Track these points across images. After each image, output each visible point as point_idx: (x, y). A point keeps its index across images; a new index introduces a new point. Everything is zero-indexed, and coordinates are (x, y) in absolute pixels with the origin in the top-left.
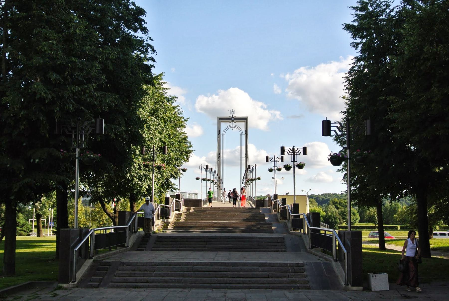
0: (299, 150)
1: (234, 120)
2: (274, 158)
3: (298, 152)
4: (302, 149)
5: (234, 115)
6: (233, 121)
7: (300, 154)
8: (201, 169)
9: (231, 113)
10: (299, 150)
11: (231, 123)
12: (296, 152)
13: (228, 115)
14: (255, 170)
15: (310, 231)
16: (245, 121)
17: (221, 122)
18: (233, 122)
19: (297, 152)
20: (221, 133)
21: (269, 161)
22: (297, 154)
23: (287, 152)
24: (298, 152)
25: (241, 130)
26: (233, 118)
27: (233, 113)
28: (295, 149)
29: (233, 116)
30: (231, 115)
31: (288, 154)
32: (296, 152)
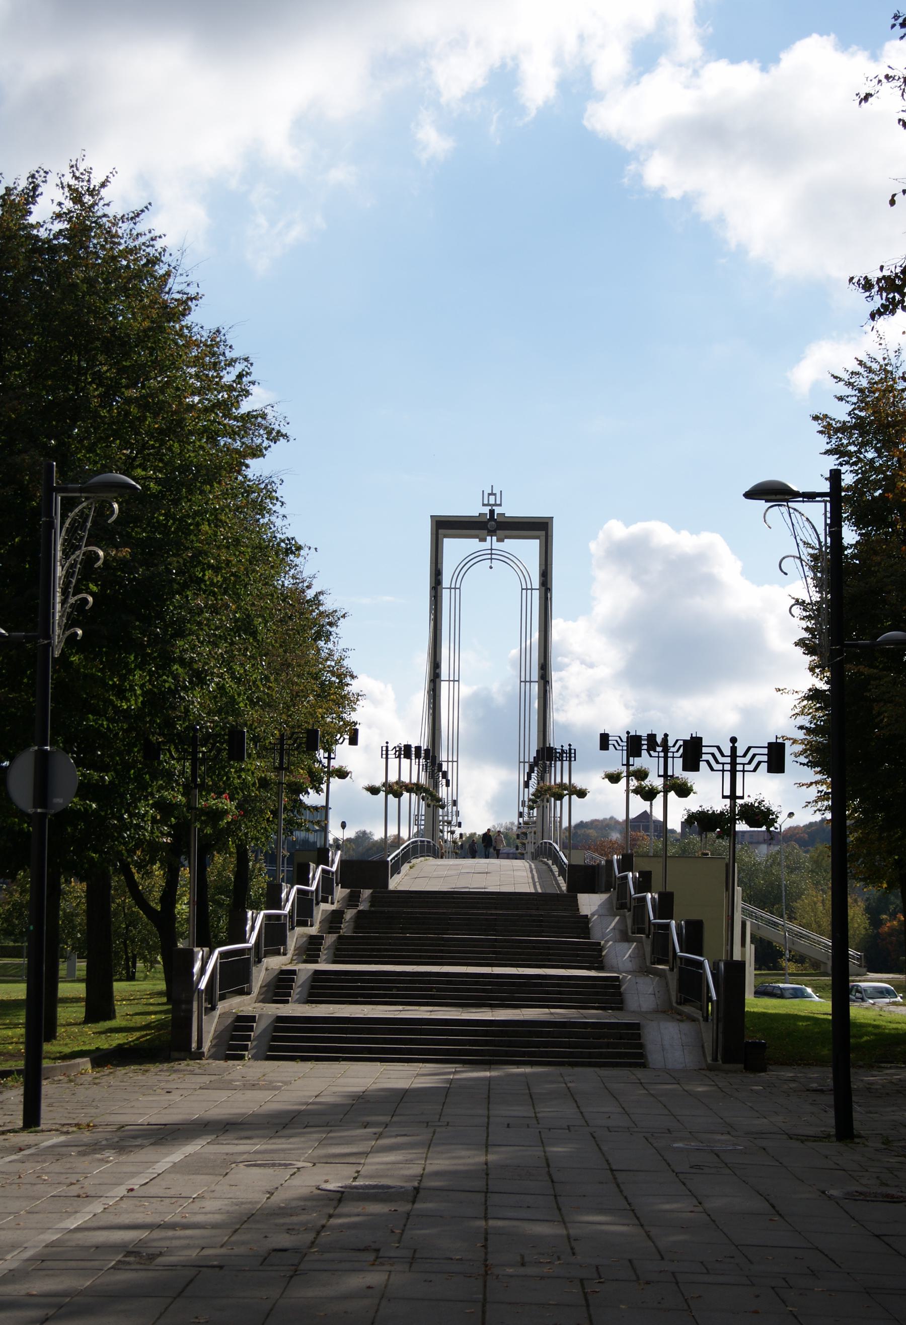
0: (754, 756)
2: (727, 752)
3: (750, 763)
4: (765, 751)
5: (498, 510)
6: (492, 533)
9: (486, 502)
10: (754, 756)
11: (484, 540)
12: (672, 749)
13: (473, 509)
15: (652, 927)
16: (543, 533)
18: (494, 538)
19: (675, 749)
21: (611, 747)
23: (614, 745)
24: (750, 763)
25: (525, 575)
27: (492, 501)
28: (670, 743)
29: (492, 512)
30: (486, 510)
31: (616, 749)
32: (672, 749)
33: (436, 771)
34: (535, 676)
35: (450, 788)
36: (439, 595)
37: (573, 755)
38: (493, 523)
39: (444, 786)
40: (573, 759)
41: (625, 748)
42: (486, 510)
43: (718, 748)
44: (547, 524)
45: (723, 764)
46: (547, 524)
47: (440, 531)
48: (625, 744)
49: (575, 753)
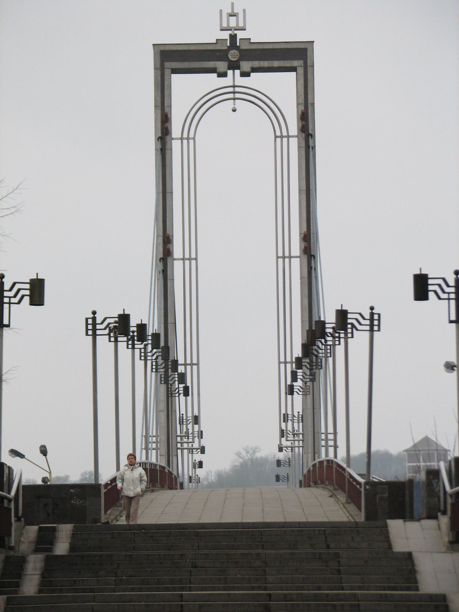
0: (19, 290)
1: (240, 59)
3: (15, 296)
4: (28, 286)
5: (240, 35)
6: (234, 66)
7: (19, 302)
8: (94, 335)
9: (225, 25)
10: (19, 290)
11: (224, 75)
14: (342, 340)
17: (175, 71)
18: (237, 72)
20: (176, 130)
21: (431, 295)
22: (10, 303)
24: (15, 296)
26: (238, 48)
27: (233, 22)
29: (233, 37)
30: (226, 35)
33: (170, 373)
34: (296, 248)
35: (189, 398)
36: (168, 147)
37: (376, 323)
38: (236, 52)
39: (182, 395)
40: (376, 328)
41: (453, 296)
42: (226, 35)
43: (444, 280)
44: (305, 50)
45: (449, 293)
46: (305, 50)
47: (168, 65)
48: (453, 290)
49: (379, 320)
